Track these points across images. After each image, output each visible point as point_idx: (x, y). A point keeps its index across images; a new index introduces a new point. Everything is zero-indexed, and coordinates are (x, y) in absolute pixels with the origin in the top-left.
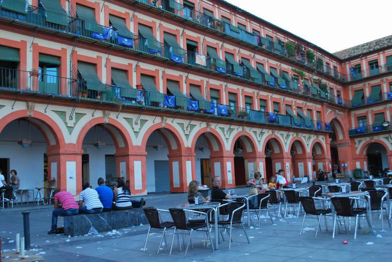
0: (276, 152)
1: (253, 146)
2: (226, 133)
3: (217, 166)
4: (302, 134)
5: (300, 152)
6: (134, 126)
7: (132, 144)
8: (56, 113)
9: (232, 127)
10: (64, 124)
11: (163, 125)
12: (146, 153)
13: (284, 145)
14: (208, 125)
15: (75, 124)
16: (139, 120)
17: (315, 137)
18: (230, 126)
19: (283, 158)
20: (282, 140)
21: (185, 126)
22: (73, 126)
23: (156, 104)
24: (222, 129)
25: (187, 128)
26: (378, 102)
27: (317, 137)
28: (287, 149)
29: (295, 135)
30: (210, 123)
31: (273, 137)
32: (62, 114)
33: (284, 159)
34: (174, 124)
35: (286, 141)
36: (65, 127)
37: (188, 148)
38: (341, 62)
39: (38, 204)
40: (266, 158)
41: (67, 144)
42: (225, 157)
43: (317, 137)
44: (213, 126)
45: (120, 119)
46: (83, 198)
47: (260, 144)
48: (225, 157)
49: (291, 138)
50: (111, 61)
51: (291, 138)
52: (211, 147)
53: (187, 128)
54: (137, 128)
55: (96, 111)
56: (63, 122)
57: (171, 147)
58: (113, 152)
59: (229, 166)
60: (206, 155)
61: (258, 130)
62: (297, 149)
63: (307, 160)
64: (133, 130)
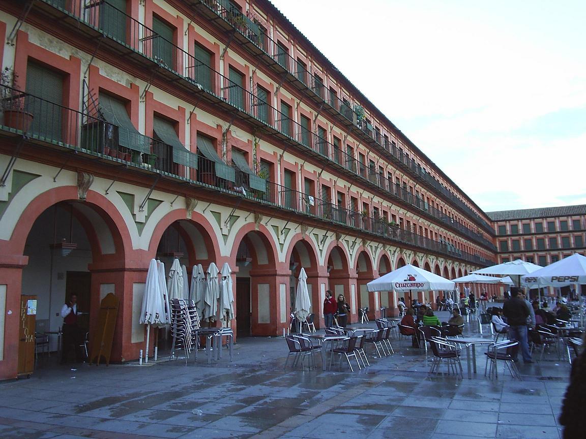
3: (263, 290)
5: (338, 266)
6: (136, 211)
9: (238, 213)
12: (23, 260)
13: (278, 247)
14: (188, 205)
16: (12, 172)
17: (251, 219)
18: (150, 194)
20: (275, 239)
22: (144, 221)
24: (217, 215)
25: (141, 207)
27: (257, 219)
28: (282, 256)
29: (299, 230)
30: (194, 201)
31: (257, 229)
32: (129, 198)
33: (126, 274)
34: (205, 212)
35: (351, 251)
37: (140, 251)
38: (491, 221)
39: (186, 365)
41: (222, 257)
42: (320, 277)
43: (303, 231)
44: (264, 220)
45: (108, 192)
47: (140, 232)
48: (320, 277)
49: (240, 224)
51: (240, 224)
53: (141, 207)
54: (282, 237)
55: (272, 218)
58: (82, 267)
61: (226, 212)
62: (301, 259)
63: (278, 279)
64: (134, 219)
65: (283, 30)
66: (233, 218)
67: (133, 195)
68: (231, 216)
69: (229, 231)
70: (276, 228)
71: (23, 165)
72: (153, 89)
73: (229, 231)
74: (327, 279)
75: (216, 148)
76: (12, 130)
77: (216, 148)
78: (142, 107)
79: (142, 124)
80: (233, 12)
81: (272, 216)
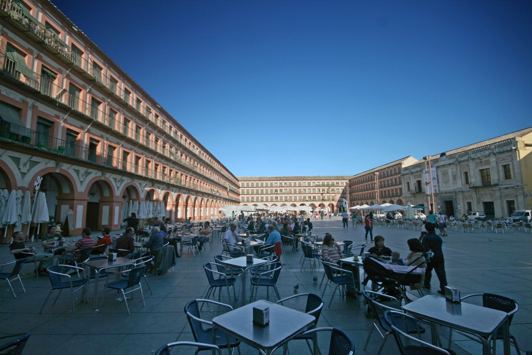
0: (105, 195)
1: (72, 188)
2: (80, 176)
3: (105, 209)
4: (110, 174)
7: (77, 190)
8: (13, 160)
9: (90, 170)
10: (17, 169)
11: (132, 184)
15: (28, 170)
18: (31, 158)
19: (113, 202)
21: (22, 162)
23: (25, 139)
24: (77, 172)
26: (54, 71)
28: (118, 192)
31: (103, 179)
32: (17, 161)
36: (19, 172)
40: (89, 203)
42: (76, 200)
44: (108, 175)
46: (496, 185)
47: (118, 190)
49: (124, 184)
50: (39, 109)
51: (124, 184)
52: (102, 193)
54: (119, 184)
56: (16, 167)
57: (62, 191)
59: (81, 210)
60: (96, 199)
65: (58, 19)
66: (87, 174)
67: (19, 159)
68: (86, 172)
69: (84, 179)
70: (115, 179)
71: (35, 159)
72: (37, 104)
73: (84, 179)
74: (76, 198)
75: (20, 116)
76: (25, 144)
77: (20, 116)
78: (29, 113)
79: (29, 122)
80: (12, 5)
81: (73, 164)
